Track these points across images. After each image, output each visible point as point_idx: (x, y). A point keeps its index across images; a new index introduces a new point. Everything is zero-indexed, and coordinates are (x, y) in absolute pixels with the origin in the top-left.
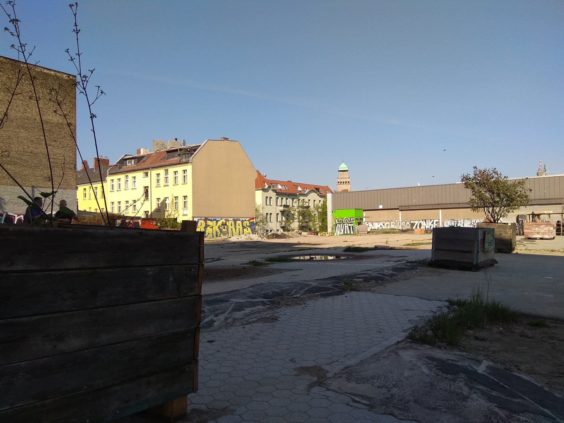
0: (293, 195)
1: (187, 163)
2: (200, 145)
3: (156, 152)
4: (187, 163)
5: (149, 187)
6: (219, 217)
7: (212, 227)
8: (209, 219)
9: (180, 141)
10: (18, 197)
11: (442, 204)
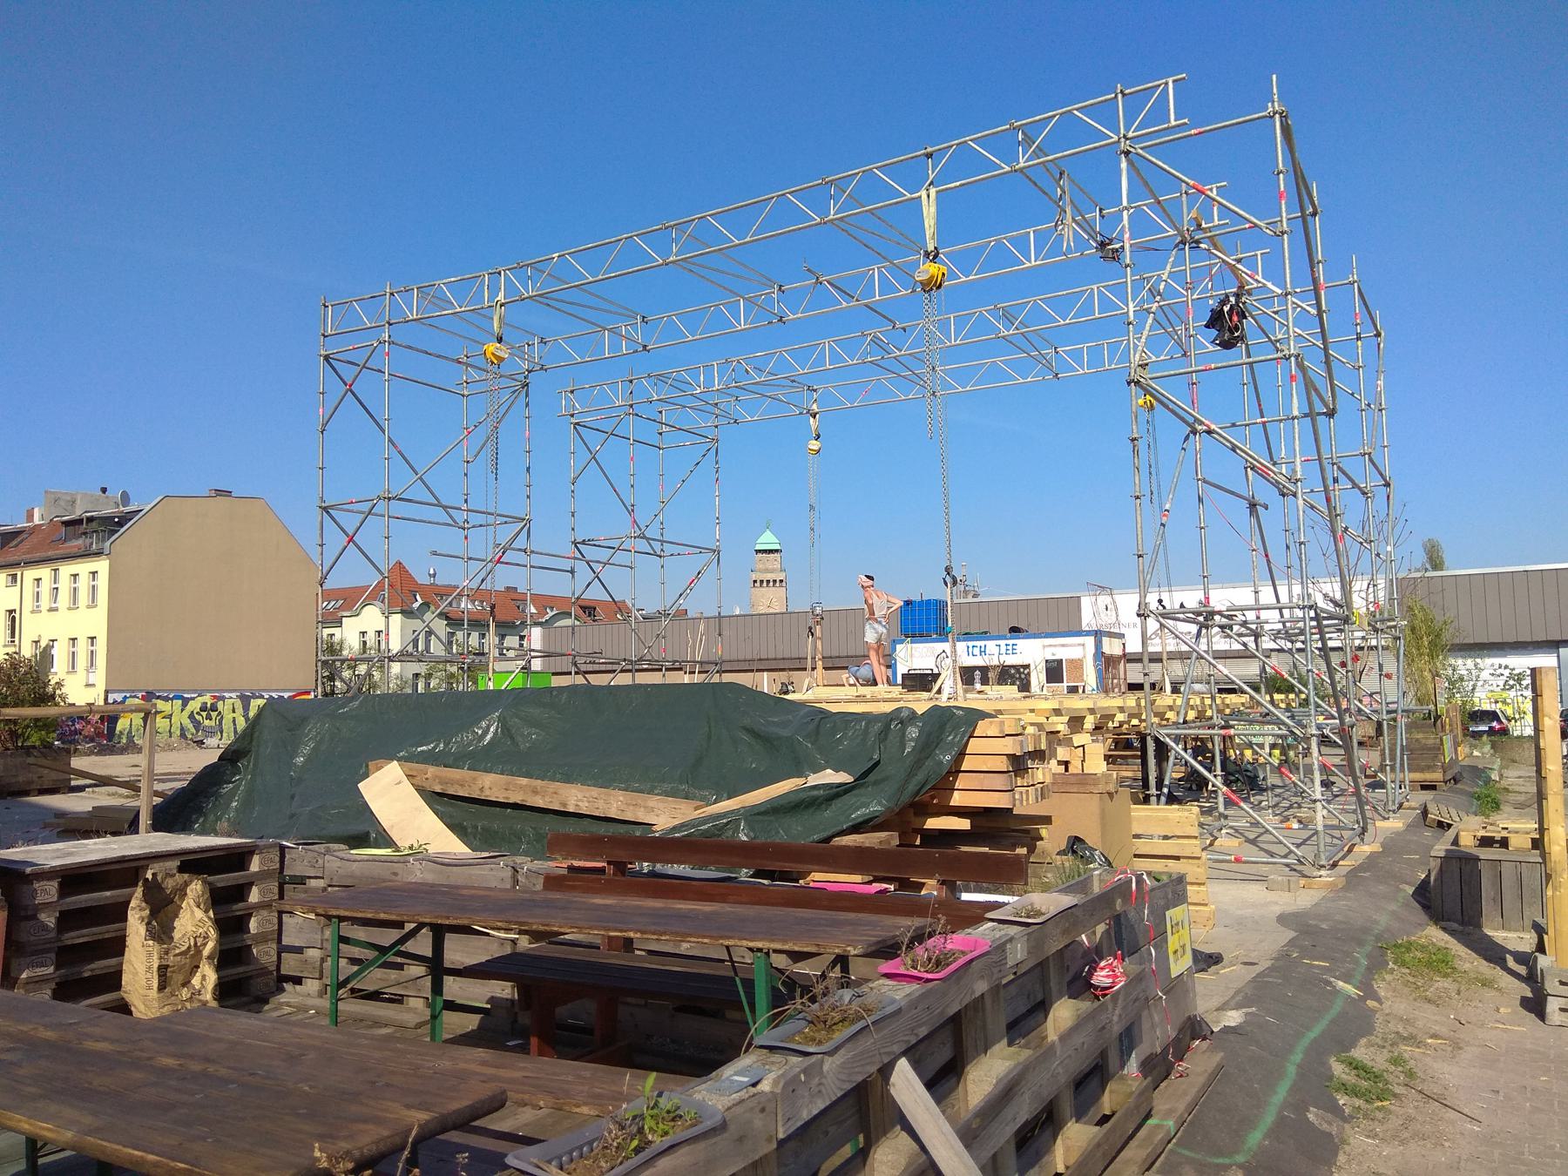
0: (503, 626)
1: (99, 554)
2: (141, 510)
3: (51, 520)
4: (98, 553)
5: (18, 612)
6: (194, 691)
7: (170, 717)
8: (159, 696)
9: (115, 493)
11: (767, 659)
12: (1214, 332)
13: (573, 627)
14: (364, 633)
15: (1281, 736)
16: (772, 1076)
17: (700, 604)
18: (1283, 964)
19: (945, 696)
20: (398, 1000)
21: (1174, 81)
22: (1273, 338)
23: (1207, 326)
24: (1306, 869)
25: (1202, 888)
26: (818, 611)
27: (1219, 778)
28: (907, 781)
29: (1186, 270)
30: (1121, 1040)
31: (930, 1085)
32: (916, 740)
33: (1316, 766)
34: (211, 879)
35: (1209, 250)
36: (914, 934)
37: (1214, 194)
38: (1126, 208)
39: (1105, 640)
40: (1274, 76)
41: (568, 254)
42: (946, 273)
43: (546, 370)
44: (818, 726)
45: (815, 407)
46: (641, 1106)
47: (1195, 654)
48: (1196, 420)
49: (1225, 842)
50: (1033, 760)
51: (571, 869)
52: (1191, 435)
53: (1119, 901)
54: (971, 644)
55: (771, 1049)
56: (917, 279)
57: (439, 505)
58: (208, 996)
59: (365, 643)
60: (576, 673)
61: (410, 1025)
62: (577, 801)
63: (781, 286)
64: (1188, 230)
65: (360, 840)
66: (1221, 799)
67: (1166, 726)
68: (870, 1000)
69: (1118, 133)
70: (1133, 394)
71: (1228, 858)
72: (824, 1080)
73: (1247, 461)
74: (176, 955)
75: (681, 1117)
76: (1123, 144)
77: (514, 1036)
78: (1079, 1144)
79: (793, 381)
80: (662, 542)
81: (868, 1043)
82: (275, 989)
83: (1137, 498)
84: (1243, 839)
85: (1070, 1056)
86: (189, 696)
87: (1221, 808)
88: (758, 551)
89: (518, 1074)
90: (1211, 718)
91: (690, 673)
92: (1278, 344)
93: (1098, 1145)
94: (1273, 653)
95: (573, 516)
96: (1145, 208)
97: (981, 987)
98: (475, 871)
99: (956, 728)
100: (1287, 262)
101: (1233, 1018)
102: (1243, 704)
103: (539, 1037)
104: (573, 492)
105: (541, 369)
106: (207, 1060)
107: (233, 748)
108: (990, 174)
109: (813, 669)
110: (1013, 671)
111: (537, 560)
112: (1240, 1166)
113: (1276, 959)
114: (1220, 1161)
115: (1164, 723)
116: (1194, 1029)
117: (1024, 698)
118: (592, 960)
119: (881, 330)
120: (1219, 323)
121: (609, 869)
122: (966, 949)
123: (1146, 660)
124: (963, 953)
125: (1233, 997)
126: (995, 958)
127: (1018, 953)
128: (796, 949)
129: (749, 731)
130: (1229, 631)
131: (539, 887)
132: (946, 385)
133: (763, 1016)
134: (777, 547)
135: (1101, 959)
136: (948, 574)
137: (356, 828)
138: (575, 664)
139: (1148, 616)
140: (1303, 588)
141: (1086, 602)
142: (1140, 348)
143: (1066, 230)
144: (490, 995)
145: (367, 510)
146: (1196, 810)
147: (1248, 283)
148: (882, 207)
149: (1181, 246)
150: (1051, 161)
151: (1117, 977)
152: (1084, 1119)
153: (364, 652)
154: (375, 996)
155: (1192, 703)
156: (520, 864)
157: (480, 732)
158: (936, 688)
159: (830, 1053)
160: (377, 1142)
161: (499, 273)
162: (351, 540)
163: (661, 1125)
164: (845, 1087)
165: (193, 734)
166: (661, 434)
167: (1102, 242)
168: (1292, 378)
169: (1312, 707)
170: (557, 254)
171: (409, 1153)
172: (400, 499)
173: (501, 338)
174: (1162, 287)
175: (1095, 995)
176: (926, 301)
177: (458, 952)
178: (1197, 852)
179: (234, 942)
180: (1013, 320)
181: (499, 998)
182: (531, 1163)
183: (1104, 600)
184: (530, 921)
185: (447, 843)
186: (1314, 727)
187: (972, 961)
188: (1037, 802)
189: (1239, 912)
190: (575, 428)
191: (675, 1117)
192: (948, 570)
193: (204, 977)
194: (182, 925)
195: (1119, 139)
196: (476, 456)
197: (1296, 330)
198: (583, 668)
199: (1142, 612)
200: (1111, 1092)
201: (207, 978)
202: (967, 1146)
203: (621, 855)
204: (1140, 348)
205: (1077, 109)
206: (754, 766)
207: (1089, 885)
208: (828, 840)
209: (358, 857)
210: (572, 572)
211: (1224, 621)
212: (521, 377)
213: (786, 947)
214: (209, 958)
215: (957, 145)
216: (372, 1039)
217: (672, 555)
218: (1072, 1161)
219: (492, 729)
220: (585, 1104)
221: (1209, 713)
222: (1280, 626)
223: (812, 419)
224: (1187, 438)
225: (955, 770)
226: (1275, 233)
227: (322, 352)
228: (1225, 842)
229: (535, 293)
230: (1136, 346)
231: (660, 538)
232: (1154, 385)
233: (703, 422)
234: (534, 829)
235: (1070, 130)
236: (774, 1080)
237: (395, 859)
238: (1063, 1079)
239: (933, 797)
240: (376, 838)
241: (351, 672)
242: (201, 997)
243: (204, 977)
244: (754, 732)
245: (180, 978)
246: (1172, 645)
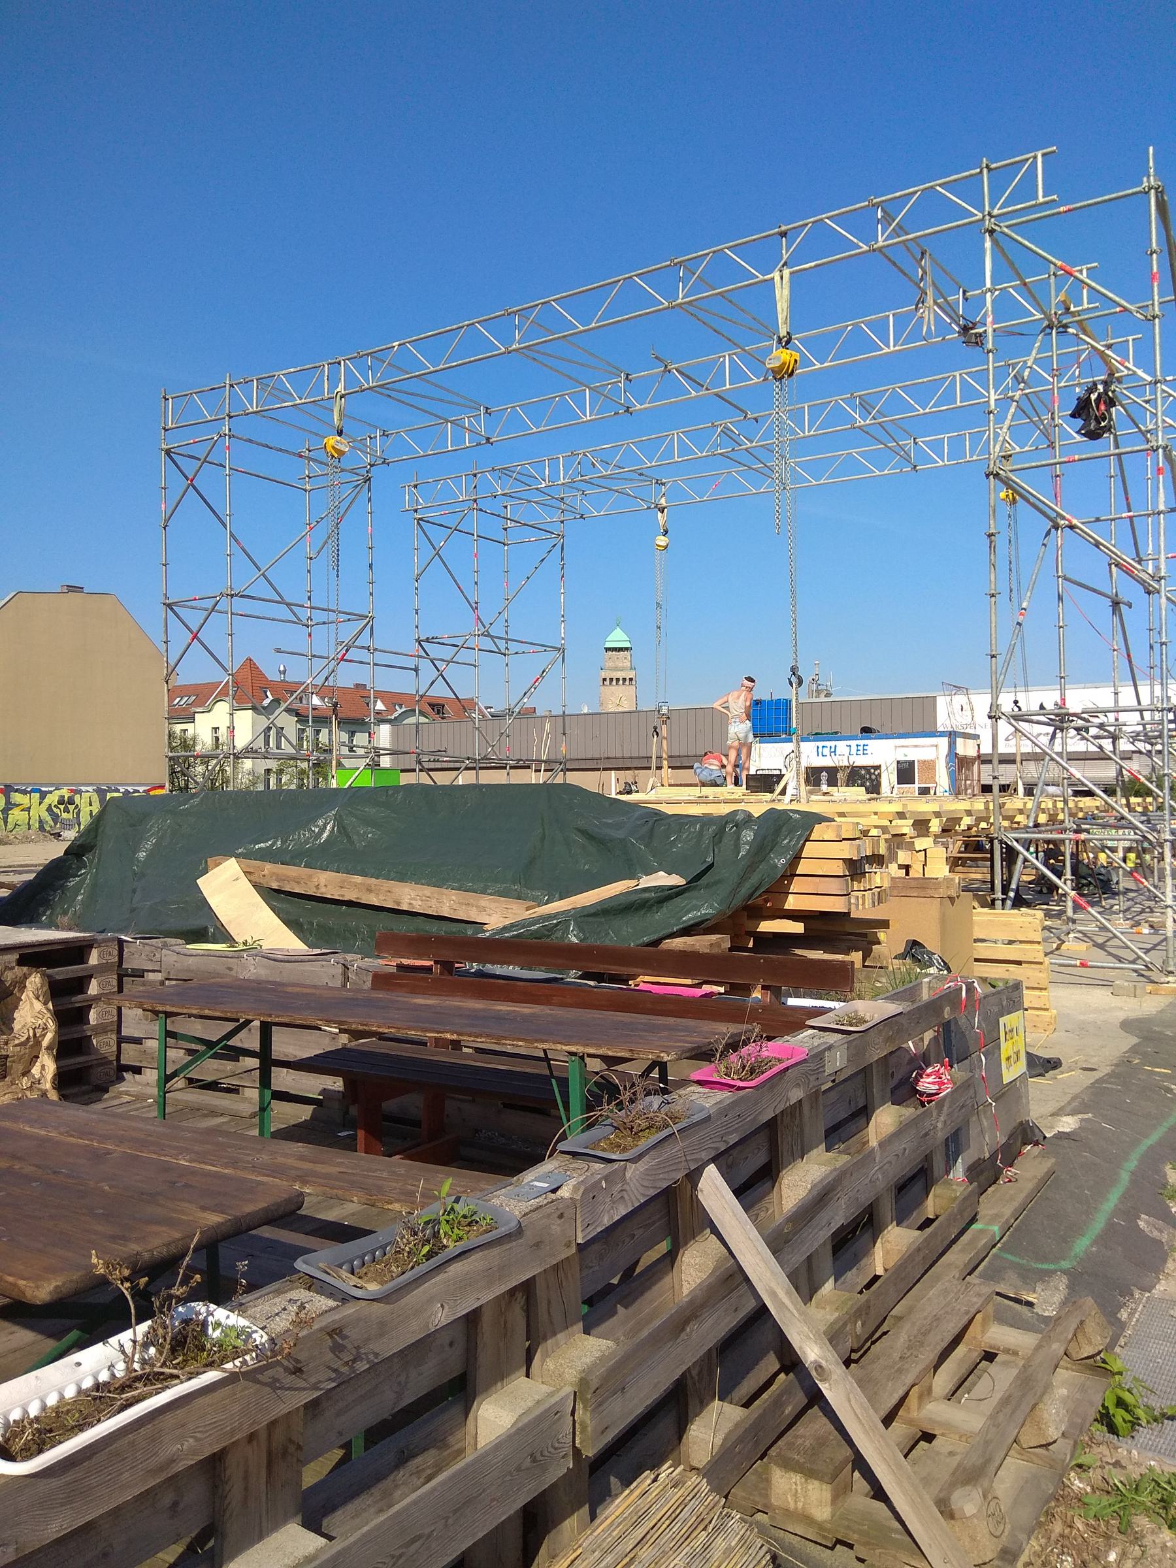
0: (353, 723)
6: (52, 785)
7: (28, 809)
10: (351, 1440)
11: (615, 758)
12: (1079, 422)
13: (417, 725)
14: (216, 729)
15: (1137, 841)
16: (573, 1182)
17: (545, 702)
18: (1124, 1070)
19: (787, 798)
20: (233, 1090)
21: (1043, 155)
22: (1143, 428)
23: (1073, 416)
24: (1154, 975)
25: (1044, 993)
26: (664, 710)
27: (1069, 882)
28: (739, 885)
29: (1052, 356)
30: (947, 1145)
31: (738, 1192)
32: (750, 843)
33: (1168, 872)
34: (50, 971)
35: (1077, 335)
36: (730, 1041)
37: (1084, 276)
38: (990, 290)
39: (959, 741)
40: (1151, 149)
41: (409, 342)
42: (798, 359)
43: (388, 464)
44: (652, 829)
45: (663, 501)
46: (435, 1210)
47: (1048, 758)
48: (1058, 514)
49: (1073, 946)
50: (871, 864)
51: (400, 967)
52: (1053, 530)
53: (947, 1009)
54: (821, 744)
55: (575, 1154)
56: (768, 366)
57: (283, 602)
58: (47, 1085)
59: (217, 739)
60: (421, 770)
61: (244, 1115)
62: (410, 899)
63: (628, 375)
64: (1055, 314)
65: (199, 935)
66: (1070, 904)
67: (1017, 829)
68: (676, 1108)
69: (982, 211)
70: (992, 487)
71: (1073, 962)
72: (626, 1187)
73: (1111, 558)
74: (16, 1046)
75: (477, 1222)
76: (987, 222)
77: (344, 1127)
78: (898, 1248)
79: (641, 474)
80: (507, 640)
81: (675, 1150)
82: (114, 1078)
83: (992, 596)
84: (1091, 943)
85: (890, 1162)
86: (46, 789)
87: (1070, 913)
88: (607, 649)
89: (334, 1170)
90: (1063, 821)
91: (536, 771)
92: (1149, 435)
93: (918, 1250)
94: (1134, 755)
95: (417, 613)
96: (1011, 290)
97: (796, 1095)
98: (307, 967)
99: (791, 831)
100: (1158, 348)
101: (1068, 1124)
102: (1097, 808)
103: (366, 1131)
104: (417, 589)
105: (384, 463)
106: (14, 1157)
107: (78, 843)
108: (847, 254)
109: (659, 768)
110: (863, 772)
111: (380, 658)
112: (1064, 1272)
113: (1117, 1065)
114: (1045, 1266)
115: (1016, 826)
116: (1026, 1134)
117: (869, 800)
118: (413, 1055)
119: (731, 422)
120: (1086, 411)
121: (436, 968)
122: (784, 1057)
123: (995, 761)
124: (780, 1061)
125: (1069, 1103)
126: (812, 1066)
127: (837, 1061)
128: (610, 1054)
129: (583, 832)
130: (1084, 734)
131: (369, 984)
132: (796, 478)
133: (577, 1117)
134: (627, 645)
135: (928, 1066)
136: (794, 674)
137: (195, 923)
138: (420, 762)
139: (1000, 718)
140: (1163, 690)
141: (941, 702)
142: (1001, 438)
143: (927, 312)
144: (322, 1087)
145: (210, 607)
146: (1040, 914)
147: (1118, 371)
148: (733, 289)
149: (1048, 331)
150: (911, 239)
151: (944, 1084)
152: (905, 1223)
153: (217, 748)
154: (213, 1086)
155: (1043, 806)
156: (351, 961)
157: (317, 830)
158: (779, 789)
159: (634, 1160)
160: (168, 1245)
161: (339, 363)
162: (195, 637)
163: (456, 1230)
164: (649, 1193)
165: (51, 827)
166: (505, 529)
167: (965, 326)
168: (1159, 471)
169: (1167, 812)
170: (397, 343)
171: (190, 1259)
172: (242, 596)
173: (342, 431)
174: (1026, 373)
175: (921, 1101)
176: (777, 390)
177: (286, 1045)
178: (1040, 957)
179: (74, 1033)
180: (870, 410)
181: (330, 1090)
182: (319, 1268)
183: (960, 699)
184: (349, 1020)
185: (287, 941)
186: (1168, 833)
187: (787, 1069)
188: (874, 906)
189: (1082, 1017)
190: (418, 523)
191: (472, 1222)
192: (794, 670)
193: (43, 1067)
194: (21, 1016)
195: (984, 216)
196: (319, 553)
197: (1167, 420)
198: (426, 765)
199: (993, 714)
200: (935, 1196)
201: (45, 1068)
202: (775, 1252)
203: (447, 955)
204: (1001, 438)
205: (940, 185)
206: (587, 867)
207: (918, 993)
208: (656, 943)
209: (194, 952)
210: (416, 670)
211: (1080, 723)
212: (363, 472)
213: (600, 1052)
214: (47, 1048)
215: (813, 222)
216: (195, 1132)
217: (516, 653)
218: (890, 1265)
219: (328, 828)
220: (398, 1201)
221: (1061, 817)
222: (1140, 728)
223: (660, 514)
224: (1048, 533)
225: (790, 874)
226: (1146, 317)
227: (164, 446)
228: (1073, 946)
229: (375, 384)
230: (997, 435)
231: (504, 636)
232: (1014, 478)
233: (548, 517)
234: (368, 926)
235: (933, 206)
236: (574, 1186)
237: (230, 954)
238: (881, 1184)
239: (766, 901)
240: (214, 934)
241: (204, 767)
242: (41, 1086)
243: (43, 1067)
244: (588, 834)
245: (20, 1068)
246: (1027, 747)
